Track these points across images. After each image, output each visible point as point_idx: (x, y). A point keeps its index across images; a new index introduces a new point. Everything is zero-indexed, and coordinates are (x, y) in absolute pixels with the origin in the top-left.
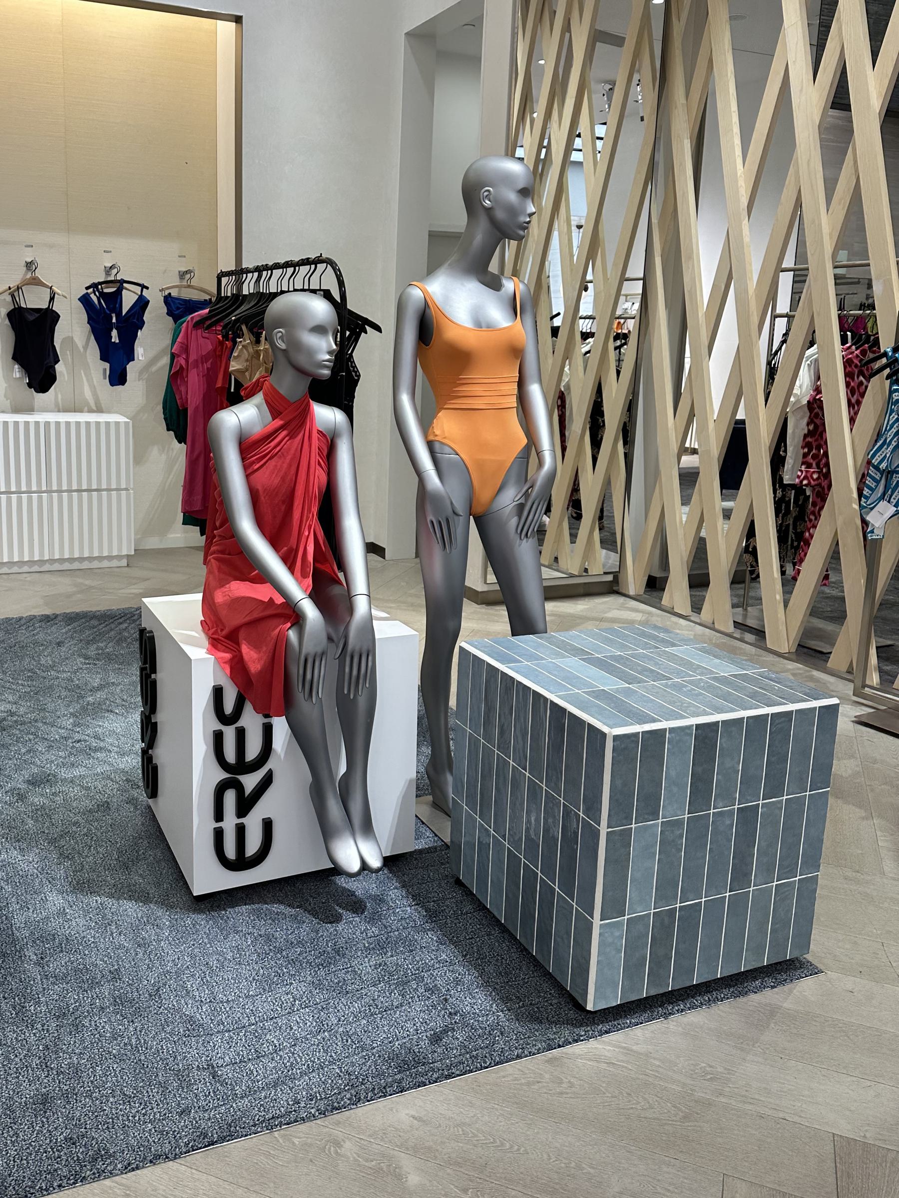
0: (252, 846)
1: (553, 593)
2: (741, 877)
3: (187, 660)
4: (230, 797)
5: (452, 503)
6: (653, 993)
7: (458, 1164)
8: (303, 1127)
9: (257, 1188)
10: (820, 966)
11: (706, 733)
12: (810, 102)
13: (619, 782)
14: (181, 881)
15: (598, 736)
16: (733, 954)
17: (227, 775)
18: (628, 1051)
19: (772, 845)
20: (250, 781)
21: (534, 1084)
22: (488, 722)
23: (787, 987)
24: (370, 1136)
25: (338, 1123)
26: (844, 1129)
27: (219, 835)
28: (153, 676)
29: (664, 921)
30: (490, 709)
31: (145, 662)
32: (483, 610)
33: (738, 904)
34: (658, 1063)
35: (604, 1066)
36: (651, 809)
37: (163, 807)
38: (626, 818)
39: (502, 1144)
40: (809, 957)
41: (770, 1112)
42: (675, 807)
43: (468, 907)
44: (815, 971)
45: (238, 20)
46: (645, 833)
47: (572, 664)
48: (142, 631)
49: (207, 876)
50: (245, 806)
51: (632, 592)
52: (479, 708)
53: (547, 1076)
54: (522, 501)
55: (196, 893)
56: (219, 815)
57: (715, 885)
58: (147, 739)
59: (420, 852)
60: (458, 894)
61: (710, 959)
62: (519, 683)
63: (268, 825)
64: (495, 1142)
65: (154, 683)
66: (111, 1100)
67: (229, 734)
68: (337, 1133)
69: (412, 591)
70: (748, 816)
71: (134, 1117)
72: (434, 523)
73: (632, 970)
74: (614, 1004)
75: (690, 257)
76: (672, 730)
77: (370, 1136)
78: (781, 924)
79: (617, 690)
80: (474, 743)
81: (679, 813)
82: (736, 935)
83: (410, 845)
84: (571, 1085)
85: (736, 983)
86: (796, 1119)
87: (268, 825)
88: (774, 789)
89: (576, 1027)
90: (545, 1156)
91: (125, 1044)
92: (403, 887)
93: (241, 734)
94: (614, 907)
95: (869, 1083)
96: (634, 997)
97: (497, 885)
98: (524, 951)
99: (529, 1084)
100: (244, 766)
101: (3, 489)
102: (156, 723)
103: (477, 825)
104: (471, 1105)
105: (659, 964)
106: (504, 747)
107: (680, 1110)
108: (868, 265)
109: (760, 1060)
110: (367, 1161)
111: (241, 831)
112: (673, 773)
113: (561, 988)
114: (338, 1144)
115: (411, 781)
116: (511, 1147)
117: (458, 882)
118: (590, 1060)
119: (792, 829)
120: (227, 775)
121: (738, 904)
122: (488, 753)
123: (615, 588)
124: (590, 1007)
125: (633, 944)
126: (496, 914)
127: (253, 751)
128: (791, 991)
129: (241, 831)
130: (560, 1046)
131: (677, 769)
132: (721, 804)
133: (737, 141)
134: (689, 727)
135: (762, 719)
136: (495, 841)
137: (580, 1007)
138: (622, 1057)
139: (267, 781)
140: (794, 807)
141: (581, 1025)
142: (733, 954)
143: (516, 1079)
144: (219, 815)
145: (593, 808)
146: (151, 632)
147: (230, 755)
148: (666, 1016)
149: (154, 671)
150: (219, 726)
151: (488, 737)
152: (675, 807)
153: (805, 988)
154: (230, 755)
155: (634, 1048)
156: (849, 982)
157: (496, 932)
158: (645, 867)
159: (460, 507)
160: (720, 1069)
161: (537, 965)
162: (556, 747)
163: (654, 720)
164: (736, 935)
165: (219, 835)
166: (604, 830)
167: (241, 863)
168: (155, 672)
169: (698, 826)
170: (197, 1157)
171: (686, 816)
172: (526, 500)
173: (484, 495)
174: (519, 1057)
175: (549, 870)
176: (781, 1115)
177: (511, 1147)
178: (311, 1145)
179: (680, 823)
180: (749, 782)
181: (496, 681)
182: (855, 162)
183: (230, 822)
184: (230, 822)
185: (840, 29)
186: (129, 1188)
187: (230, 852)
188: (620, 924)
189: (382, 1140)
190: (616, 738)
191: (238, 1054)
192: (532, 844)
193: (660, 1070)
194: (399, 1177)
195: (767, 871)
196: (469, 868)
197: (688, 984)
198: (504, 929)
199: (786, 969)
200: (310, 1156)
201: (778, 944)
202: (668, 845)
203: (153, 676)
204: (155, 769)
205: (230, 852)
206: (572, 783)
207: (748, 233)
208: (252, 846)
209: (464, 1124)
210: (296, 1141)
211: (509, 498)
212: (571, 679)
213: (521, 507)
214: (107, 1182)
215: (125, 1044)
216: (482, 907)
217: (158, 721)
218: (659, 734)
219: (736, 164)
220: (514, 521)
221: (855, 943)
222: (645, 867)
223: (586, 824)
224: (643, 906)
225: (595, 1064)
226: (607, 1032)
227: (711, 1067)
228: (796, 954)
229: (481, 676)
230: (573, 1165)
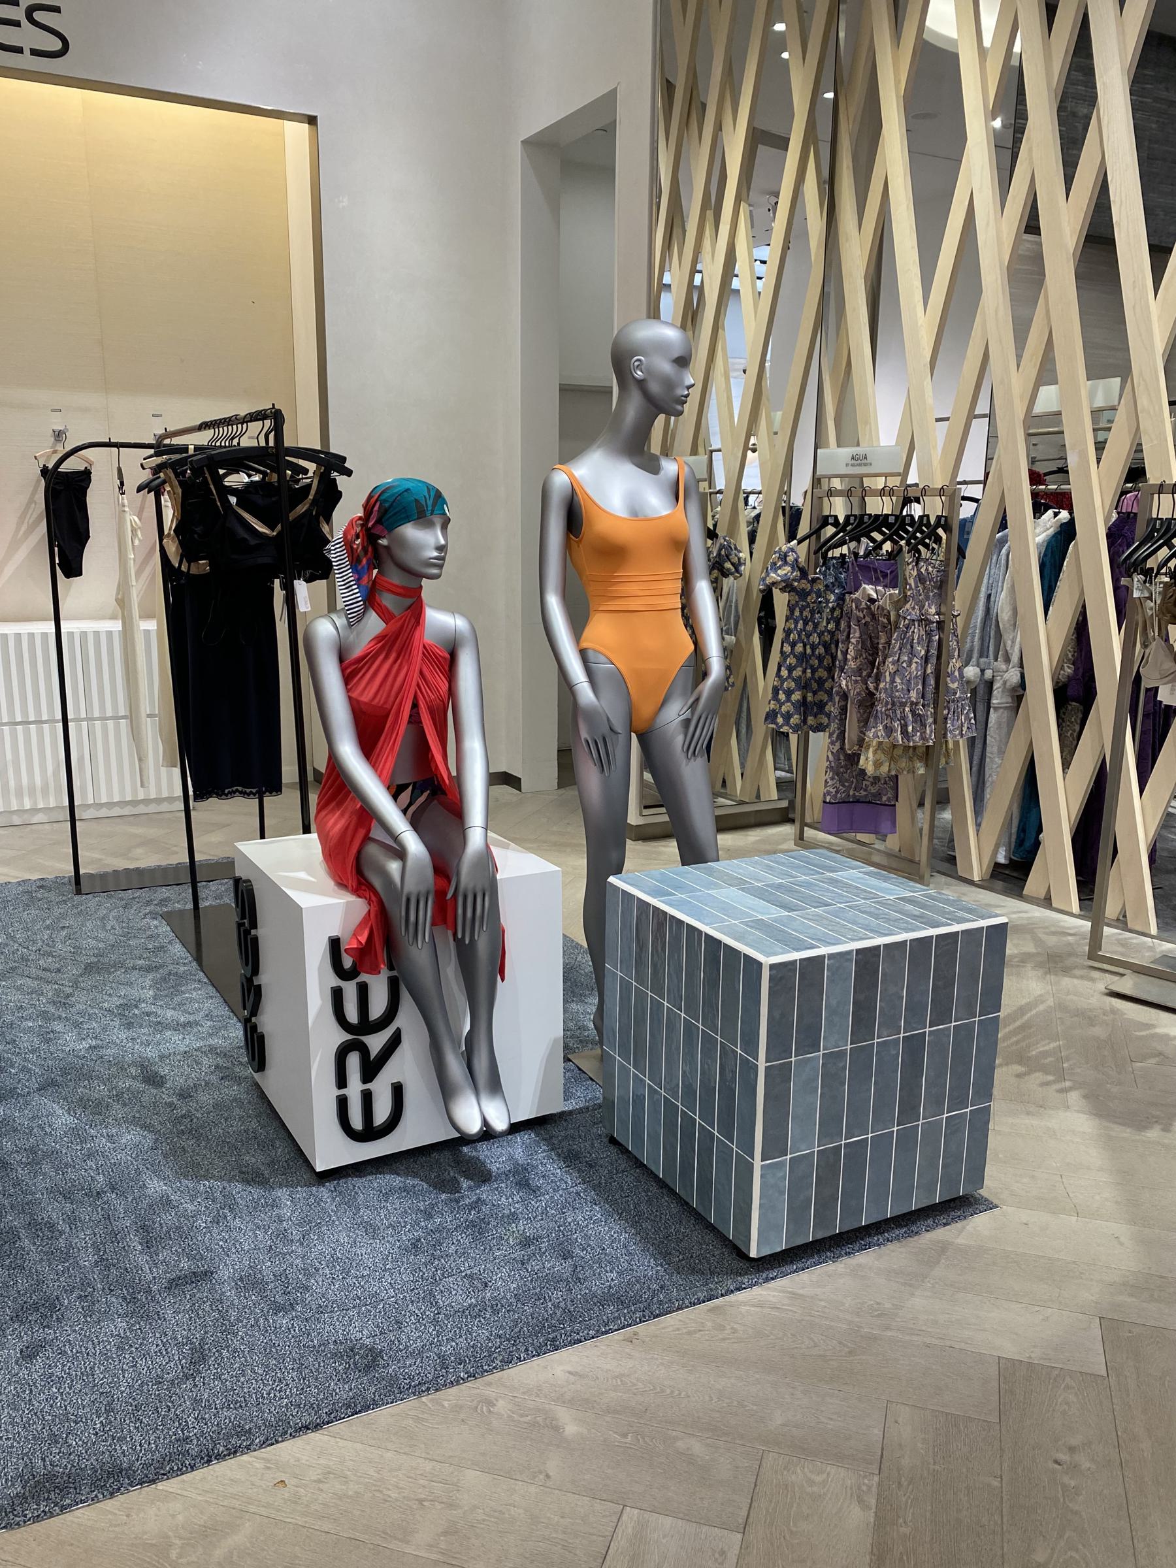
0: (382, 1113)
1: (726, 824)
2: (909, 1110)
3: (296, 911)
4: (353, 1061)
5: (608, 720)
6: (820, 1236)
7: (616, 1412)
8: (453, 1391)
9: (407, 1450)
10: (995, 1202)
11: (867, 957)
12: (996, 238)
13: (777, 1014)
14: (301, 1158)
15: (754, 966)
16: (904, 1192)
17: (350, 1037)
18: (794, 1296)
19: (941, 1075)
20: (376, 1042)
21: (695, 1332)
22: (640, 962)
23: (959, 1225)
24: (524, 1393)
25: (489, 1384)
26: (1010, 1350)
27: (342, 1103)
28: (253, 932)
29: (829, 1159)
30: (641, 947)
31: (243, 917)
32: (638, 847)
33: (907, 1139)
34: (823, 1304)
35: (767, 1311)
36: (810, 1042)
37: (273, 1082)
38: (785, 1051)
39: (663, 1391)
40: (983, 1192)
41: (937, 1342)
42: (836, 1038)
43: (623, 1164)
44: (991, 1206)
45: (312, 120)
46: (808, 1067)
47: (730, 895)
48: (237, 881)
49: (330, 1149)
50: (370, 1071)
51: (976, 878)
52: (630, 949)
53: (709, 1324)
54: (688, 715)
55: (319, 1168)
56: (342, 1082)
57: (882, 1119)
58: (249, 1005)
59: (571, 1113)
60: (613, 1151)
61: (879, 1198)
62: (672, 917)
63: (398, 1091)
64: (655, 1388)
65: (255, 940)
66: (242, 1379)
67: (350, 990)
68: (489, 1392)
69: (555, 829)
70: (914, 1045)
71: (269, 1394)
72: (576, 743)
73: (797, 1213)
74: (779, 1250)
75: (867, 422)
76: (831, 956)
77: (524, 1393)
78: (953, 1159)
79: (775, 920)
80: (625, 986)
81: (840, 1043)
82: (905, 1171)
83: (557, 1106)
84: (735, 1331)
85: (907, 1222)
86: (963, 1346)
87: (398, 1091)
88: (942, 1016)
89: (740, 1275)
90: (707, 1398)
91: (252, 1326)
92: (552, 1150)
93: (363, 990)
94: (774, 1146)
95: (1037, 1308)
96: (800, 1241)
97: (654, 1138)
98: (685, 1204)
99: (689, 1333)
100: (367, 1026)
101: (5, 720)
102: (260, 986)
103: (633, 1078)
104: (630, 1356)
105: (825, 1205)
106: (658, 988)
107: (844, 1345)
108: (1063, 432)
109: (929, 1294)
110: (522, 1416)
111: (367, 1097)
112: (834, 1002)
113: (724, 1239)
114: (490, 1403)
115: (556, 1041)
116: (672, 1392)
117: (613, 1141)
118: (754, 1306)
119: (961, 1058)
120: (350, 1037)
121: (907, 1139)
122: (641, 996)
123: (790, 816)
124: (753, 1254)
125: (798, 1185)
126: (653, 1169)
127: (378, 1007)
128: (964, 1228)
129: (367, 1097)
130: (722, 1295)
131: (837, 998)
132: (885, 1033)
133: (918, 283)
134: (849, 952)
135: (924, 942)
136: (648, 1090)
137: (743, 1256)
138: (787, 1301)
139: (395, 1042)
140: (963, 1033)
141: (746, 1274)
142: (904, 1192)
143: (678, 1329)
144: (342, 1082)
145: (751, 1044)
146: (249, 881)
147: (352, 1016)
148: (835, 1259)
149: (254, 925)
150: (335, 981)
151: (640, 979)
152: (836, 1038)
153: (979, 1224)
154: (352, 1016)
155: (801, 1292)
156: (1025, 1215)
157: (654, 1189)
158: (807, 1102)
159: (619, 726)
160: (888, 1305)
161: (700, 1219)
162: (711, 983)
163: (813, 947)
164: (905, 1171)
165: (342, 1103)
166: (762, 1064)
167: (370, 1133)
168: (256, 927)
169: (861, 1057)
170: (337, 1427)
171: (849, 1047)
172: (693, 713)
173: (645, 710)
174: (680, 1308)
175: (707, 1115)
176: (948, 1343)
177: (672, 1392)
178: (461, 1407)
179: (844, 1052)
180: (915, 1011)
181: (648, 917)
182: (1048, 311)
183: (355, 1088)
184: (355, 1088)
185: (1030, 150)
186: (268, 1461)
187: (357, 1122)
188: (783, 1163)
189: (538, 1395)
190: (772, 967)
191: (378, 1327)
192: (689, 1091)
193: (827, 1310)
194: (557, 1429)
195: (936, 1104)
196: (624, 1122)
197: (856, 1225)
198: (662, 1184)
199: (960, 1205)
200: (462, 1416)
201: (951, 1180)
202: (831, 1078)
203: (253, 932)
204: (261, 1038)
205: (357, 1122)
206: (729, 1019)
207: (931, 394)
208: (382, 1113)
209: (623, 1375)
210: (446, 1404)
211: (674, 713)
212: (726, 909)
213: (687, 722)
214: (245, 1457)
215: (252, 1326)
216: (639, 1164)
217: (262, 983)
218: (815, 963)
219: (918, 314)
220: (679, 739)
221: (1033, 1177)
222: (807, 1102)
223: (745, 1062)
224: (807, 1144)
225: (758, 1309)
226: (773, 1279)
227: (878, 1304)
228: (969, 1191)
229: (632, 912)
230: (735, 1403)
